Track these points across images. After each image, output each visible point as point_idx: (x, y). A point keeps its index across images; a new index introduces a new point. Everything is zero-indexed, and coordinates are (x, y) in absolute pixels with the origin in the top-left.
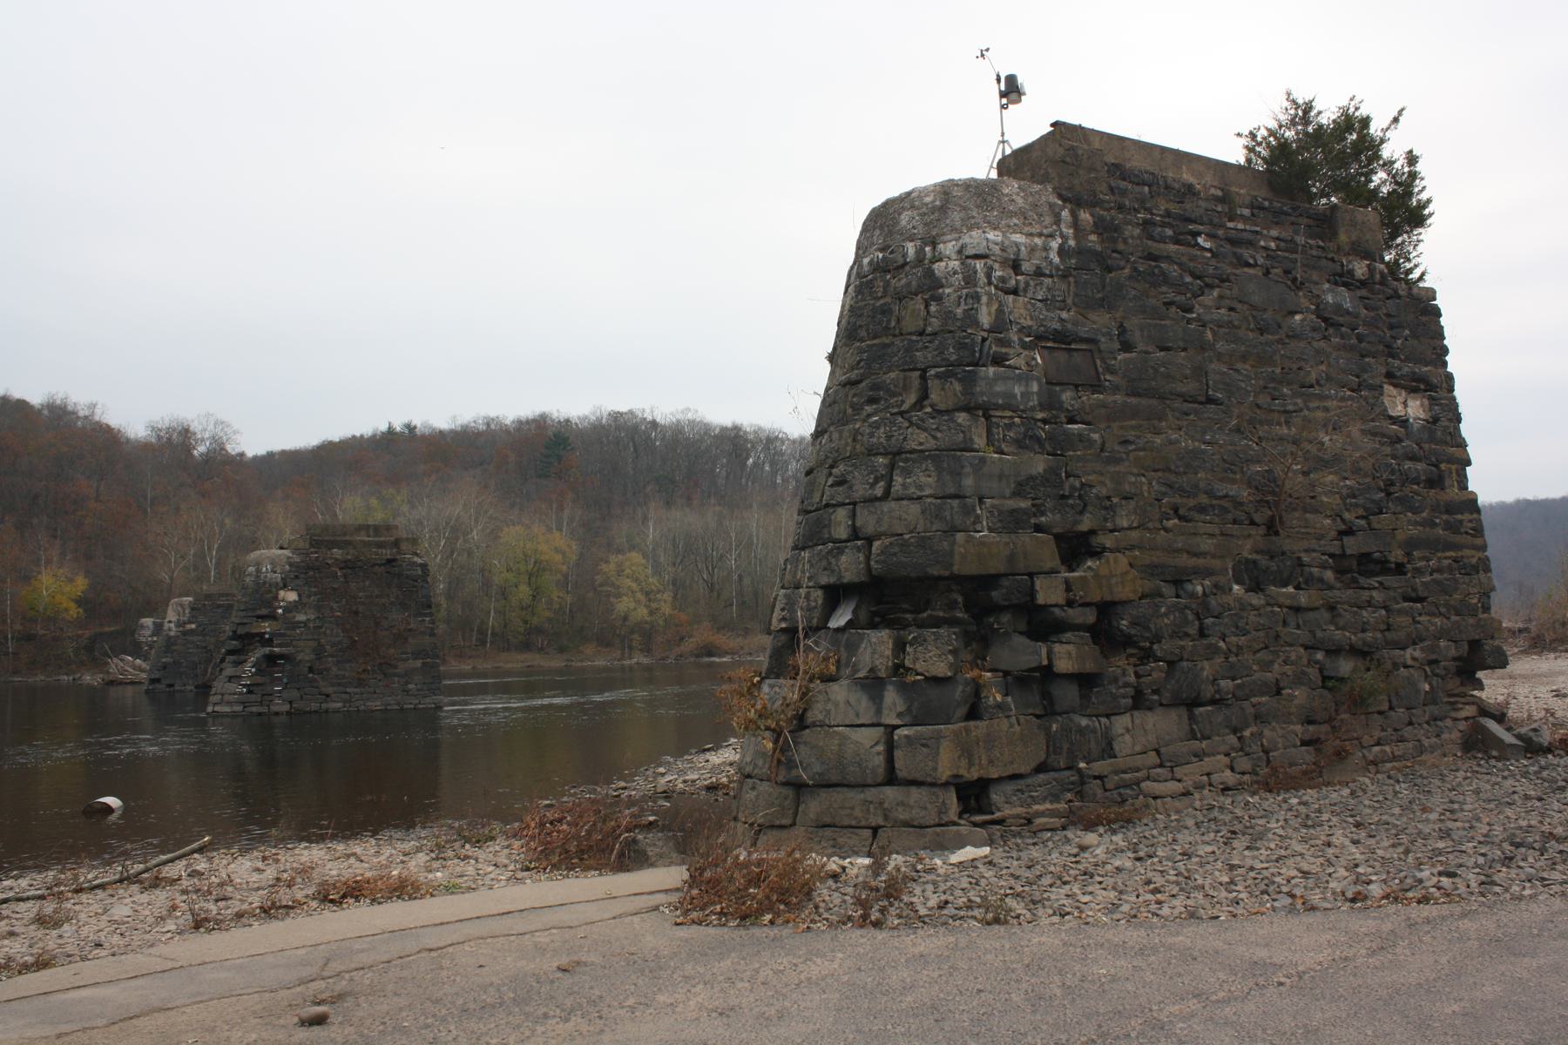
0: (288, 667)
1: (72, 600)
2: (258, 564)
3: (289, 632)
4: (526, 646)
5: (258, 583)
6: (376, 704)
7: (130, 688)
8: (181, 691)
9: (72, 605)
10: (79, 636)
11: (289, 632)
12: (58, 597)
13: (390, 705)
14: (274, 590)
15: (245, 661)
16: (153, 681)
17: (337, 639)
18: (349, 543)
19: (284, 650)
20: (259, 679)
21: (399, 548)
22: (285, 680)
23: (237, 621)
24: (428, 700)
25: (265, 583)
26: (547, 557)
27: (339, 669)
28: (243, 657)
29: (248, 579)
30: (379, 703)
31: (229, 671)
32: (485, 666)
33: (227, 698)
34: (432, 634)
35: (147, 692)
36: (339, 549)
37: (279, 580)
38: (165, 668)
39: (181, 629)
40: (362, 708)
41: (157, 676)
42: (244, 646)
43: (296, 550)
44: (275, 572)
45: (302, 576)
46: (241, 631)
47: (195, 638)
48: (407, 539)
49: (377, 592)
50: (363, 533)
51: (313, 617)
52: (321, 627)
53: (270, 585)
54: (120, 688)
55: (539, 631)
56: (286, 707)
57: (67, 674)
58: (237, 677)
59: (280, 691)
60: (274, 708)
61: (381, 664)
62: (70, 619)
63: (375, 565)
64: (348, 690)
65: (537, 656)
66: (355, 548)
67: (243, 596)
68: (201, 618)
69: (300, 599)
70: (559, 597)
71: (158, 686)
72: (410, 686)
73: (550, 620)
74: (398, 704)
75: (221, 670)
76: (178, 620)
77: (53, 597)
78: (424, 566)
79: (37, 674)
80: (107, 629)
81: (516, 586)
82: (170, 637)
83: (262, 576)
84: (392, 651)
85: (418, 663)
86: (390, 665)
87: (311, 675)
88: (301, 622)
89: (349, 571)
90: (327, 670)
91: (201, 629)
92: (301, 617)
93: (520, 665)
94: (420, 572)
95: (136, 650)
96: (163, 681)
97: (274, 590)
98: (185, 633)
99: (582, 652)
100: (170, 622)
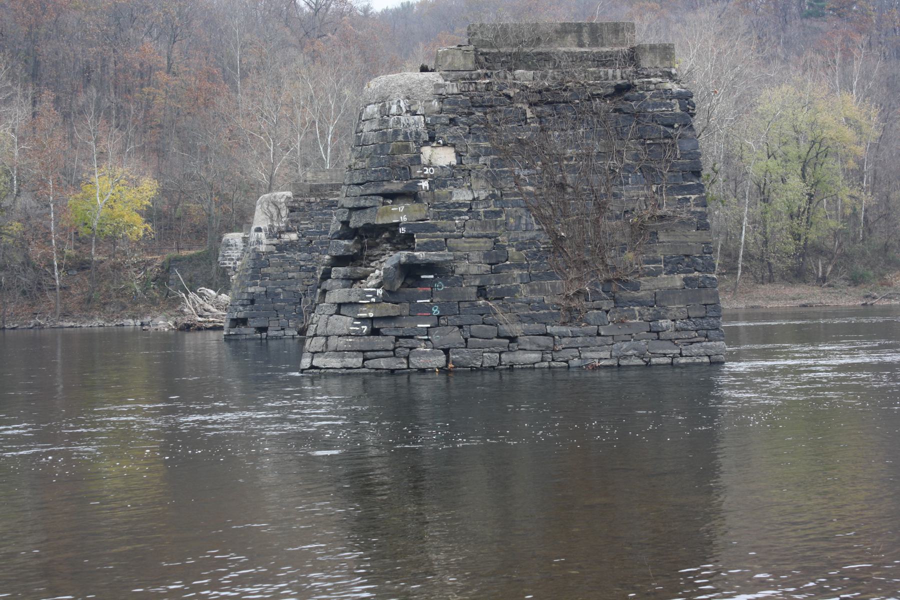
0: (440, 286)
1: (140, 213)
2: (383, 100)
3: (441, 223)
4: (798, 275)
5: (385, 134)
6: (600, 356)
7: (211, 333)
8: (277, 338)
9: (138, 219)
10: (149, 264)
11: (441, 223)
12: (119, 208)
13: (626, 357)
14: (413, 146)
15: (365, 277)
16: (237, 322)
17: (528, 235)
18: (546, 58)
19: (433, 256)
20: (389, 309)
21: (637, 66)
22: (436, 311)
23: (350, 203)
24: (695, 349)
25: (396, 133)
26: (832, 133)
27: (532, 291)
28: (360, 270)
29: (366, 127)
30: (606, 354)
31: (337, 294)
32: (735, 304)
33: (334, 342)
34: (703, 226)
35: (228, 338)
36: (529, 68)
37: (421, 127)
38: (252, 302)
39: (275, 241)
40: (576, 362)
41: (241, 315)
42: (362, 249)
43: (451, 72)
44: (414, 114)
45: (464, 119)
46: (357, 221)
47: (296, 256)
48: (653, 48)
49: (598, 148)
50: (570, 38)
51: (483, 195)
52: (498, 214)
53: (406, 136)
54: (199, 335)
55: (818, 251)
56: (440, 360)
57: (134, 318)
58: (350, 303)
59: (427, 331)
60: (418, 362)
61: (609, 281)
62: (134, 238)
63: (593, 97)
64: (549, 329)
65: (817, 290)
66: (556, 67)
67: (360, 157)
68: (305, 224)
69: (460, 163)
70: (852, 197)
71: (243, 329)
72: (663, 323)
73: (836, 234)
74: (641, 356)
75: (324, 292)
76: (271, 227)
77: (112, 207)
78: (685, 98)
79: (93, 317)
80: (184, 253)
81: (783, 181)
82: (259, 255)
83: (392, 120)
84: (629, 256)
85: (678, 280)
86: (626, 282)
87: (481, 302)
88: (462, 205)
89: (547, 109)
90: (512, 292)
91: (305, 240)
92: (462, 196)
93: (791, 304)
94: (677, 109)
95: (221, 282)
96: (251, 322)
97: (413, 146)
98: (281, 248)
99: (890, 285)
100: (259, 230)
